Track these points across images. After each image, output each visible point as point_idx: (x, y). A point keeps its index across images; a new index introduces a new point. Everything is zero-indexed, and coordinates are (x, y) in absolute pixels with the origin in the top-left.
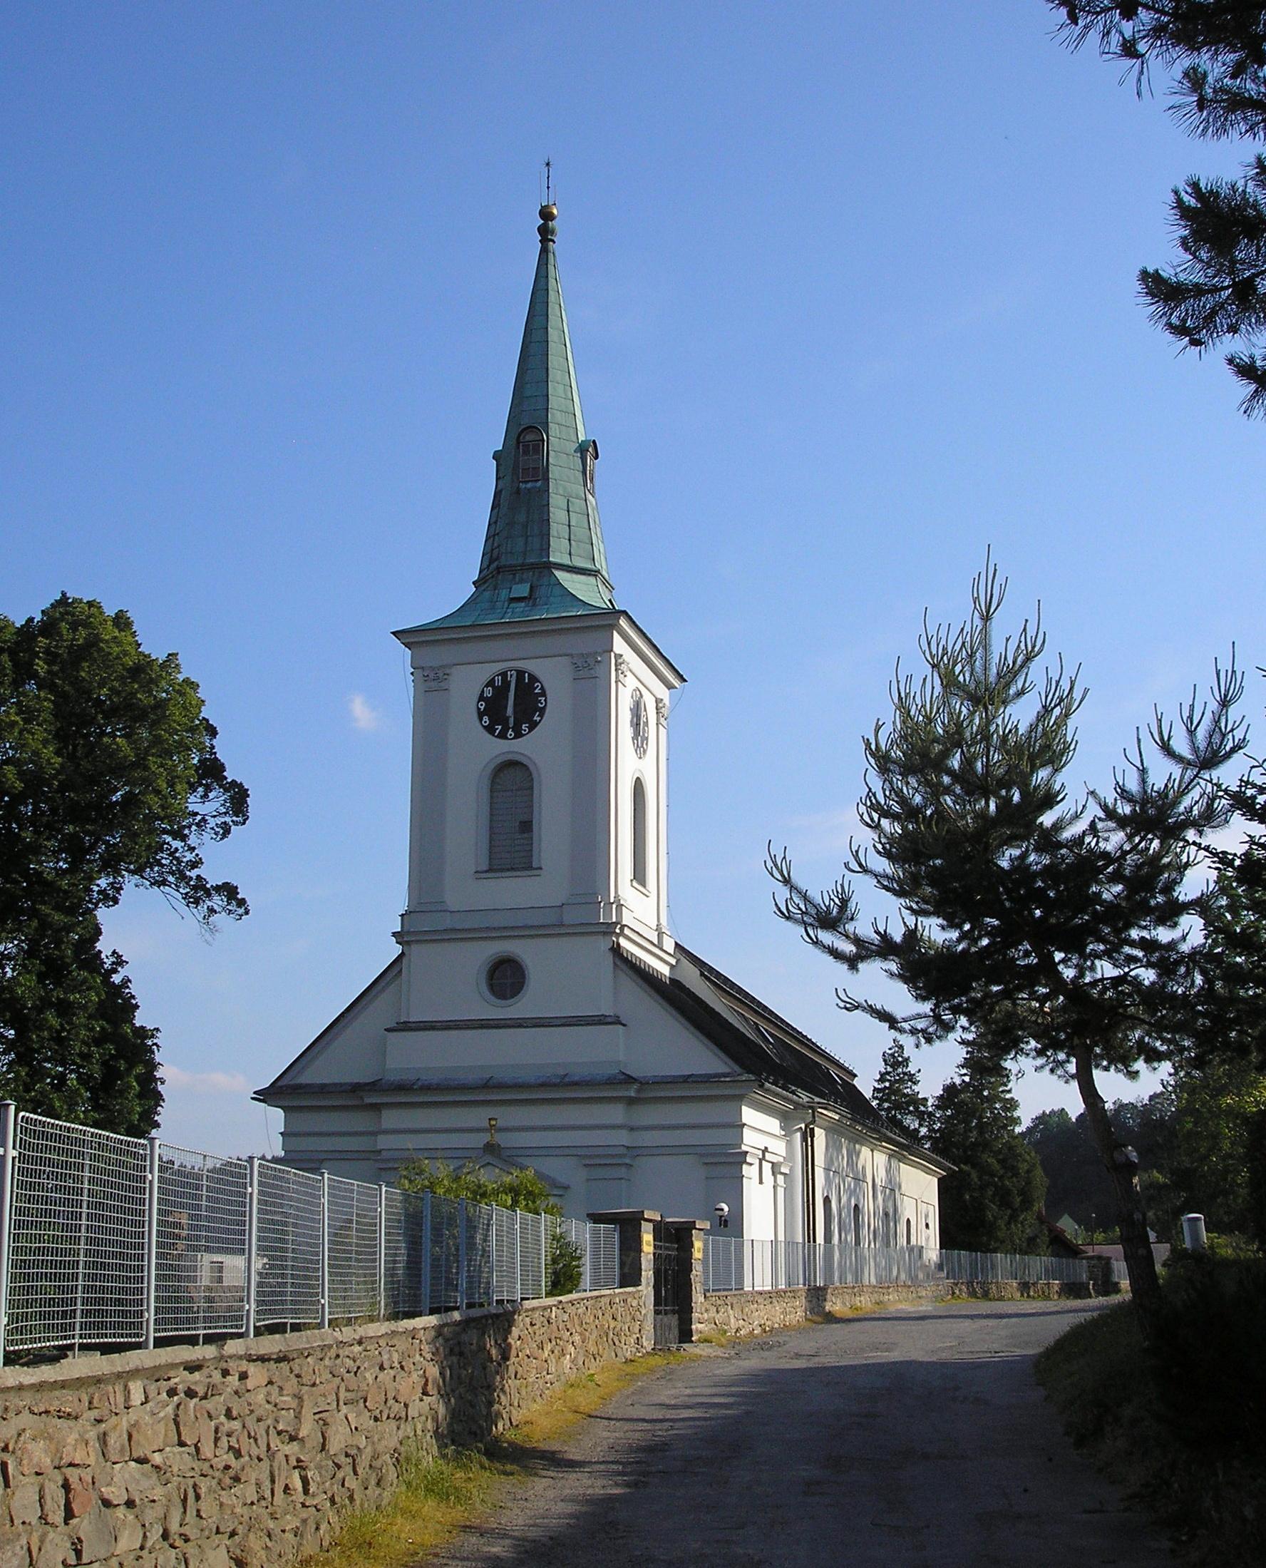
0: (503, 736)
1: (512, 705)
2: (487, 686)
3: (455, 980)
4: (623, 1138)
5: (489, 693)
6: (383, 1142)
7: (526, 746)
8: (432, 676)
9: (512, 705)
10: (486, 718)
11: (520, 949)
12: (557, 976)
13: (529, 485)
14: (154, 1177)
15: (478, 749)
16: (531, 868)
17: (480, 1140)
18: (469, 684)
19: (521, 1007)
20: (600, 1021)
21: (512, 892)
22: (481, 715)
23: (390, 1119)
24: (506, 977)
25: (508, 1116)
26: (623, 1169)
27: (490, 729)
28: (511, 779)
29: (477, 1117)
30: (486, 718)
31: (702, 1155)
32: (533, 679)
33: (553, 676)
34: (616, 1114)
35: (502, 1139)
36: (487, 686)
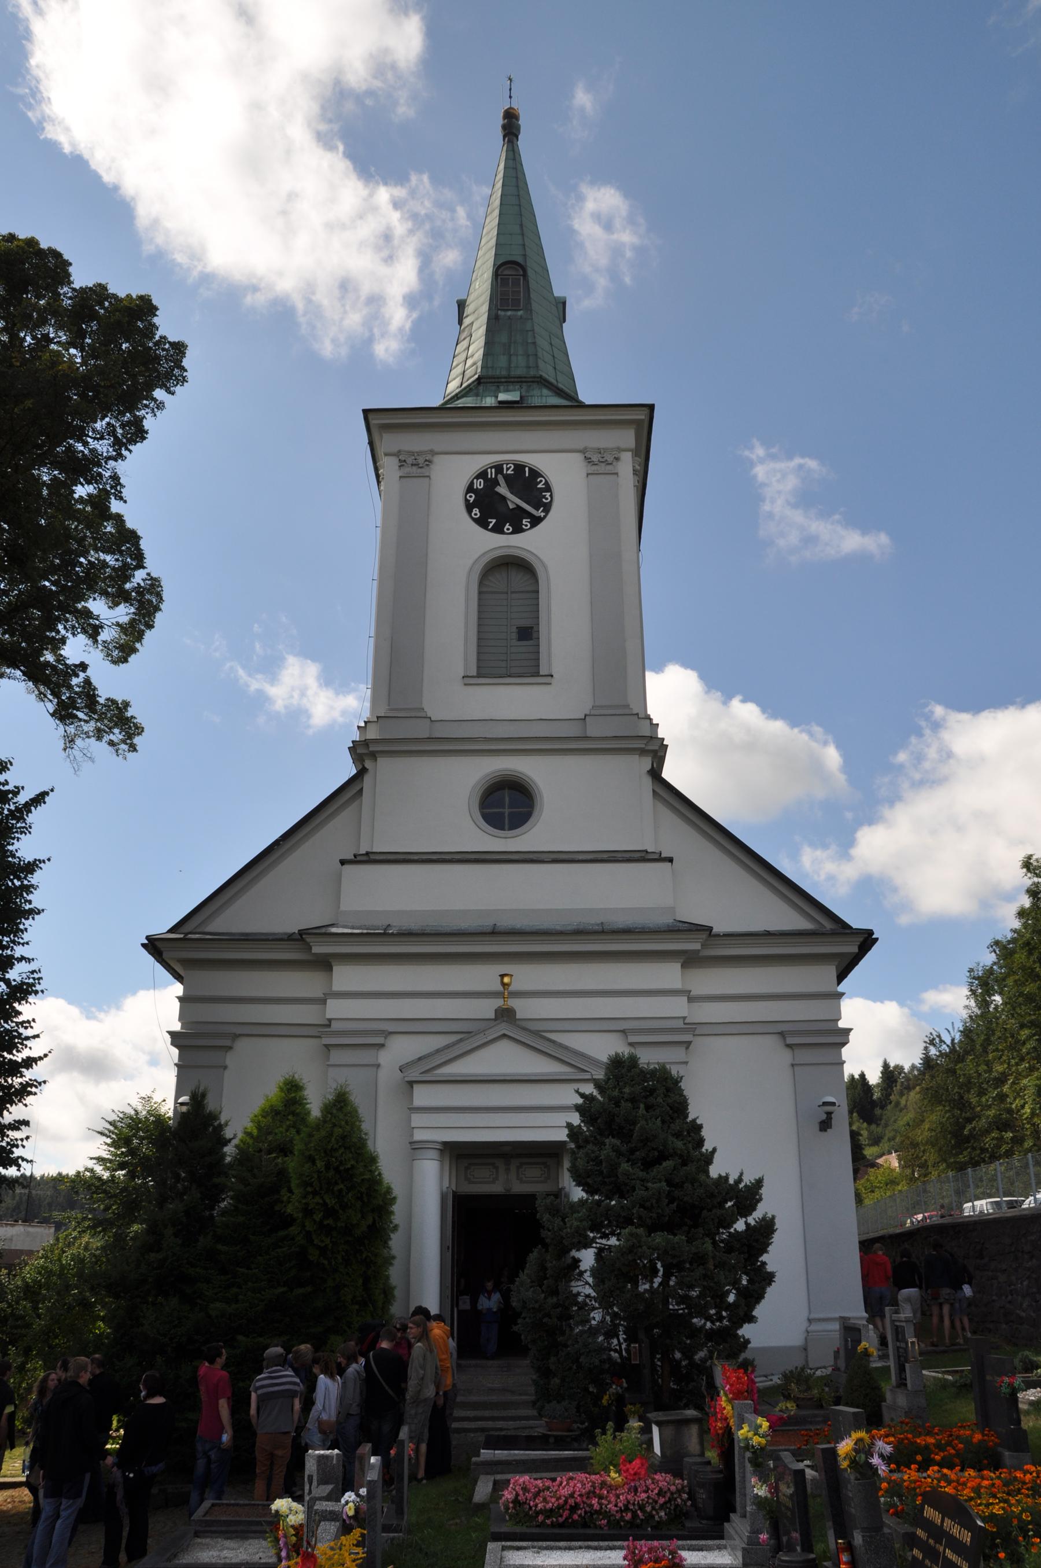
0: (498, 529)
1: (508, 500)
2: (477, 477)
3: (438, 803)
4: (677, 1007)
5: (479, 484)
6: (335, 1009)
7: (527, 542)
8: (410, 460)
9: (508, 500)
10: (476, 511)
11: (528, 767)
12: (574, 800)
13: (509, 313)
14: (832, 1445)
15: (465, 544)
16: (537, 674)
17: (486, 1008)
18: (456, 472)
19: (530, 838)
20: (643, 857)
21: (511, 702)
22: (469, 508)
23: (345, 977)
24: (508, 802)
25: (526, 976)
26: (681, 1050)
27: (482, 522)
28: (510, 578)
29: (483, 977)
30: (476, 511)
31: (623, 1032)
32: (535, 474)
33: (561, 469)
34: (670, 975)
35: (525, 1009)
36: (477, 477)
